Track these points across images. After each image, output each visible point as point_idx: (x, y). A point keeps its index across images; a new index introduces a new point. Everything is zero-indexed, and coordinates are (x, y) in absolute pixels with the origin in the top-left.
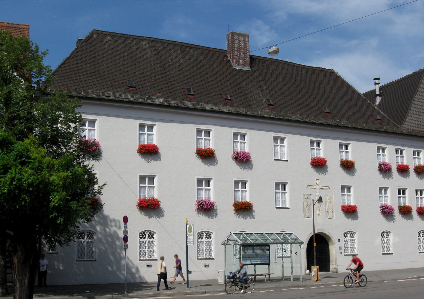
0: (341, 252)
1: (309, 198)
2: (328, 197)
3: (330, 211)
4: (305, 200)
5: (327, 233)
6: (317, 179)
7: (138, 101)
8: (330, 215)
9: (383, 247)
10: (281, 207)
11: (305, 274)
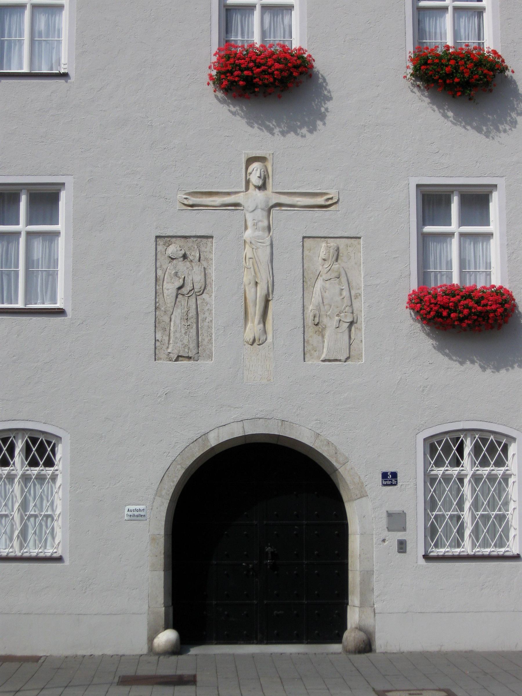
1: (194, 255)
2: (322, 249)
3: (330, 323)
4: (171, 269)
6: (250, 161)
8: (332, 341)
10: (20, 305)
11: (151, 648)
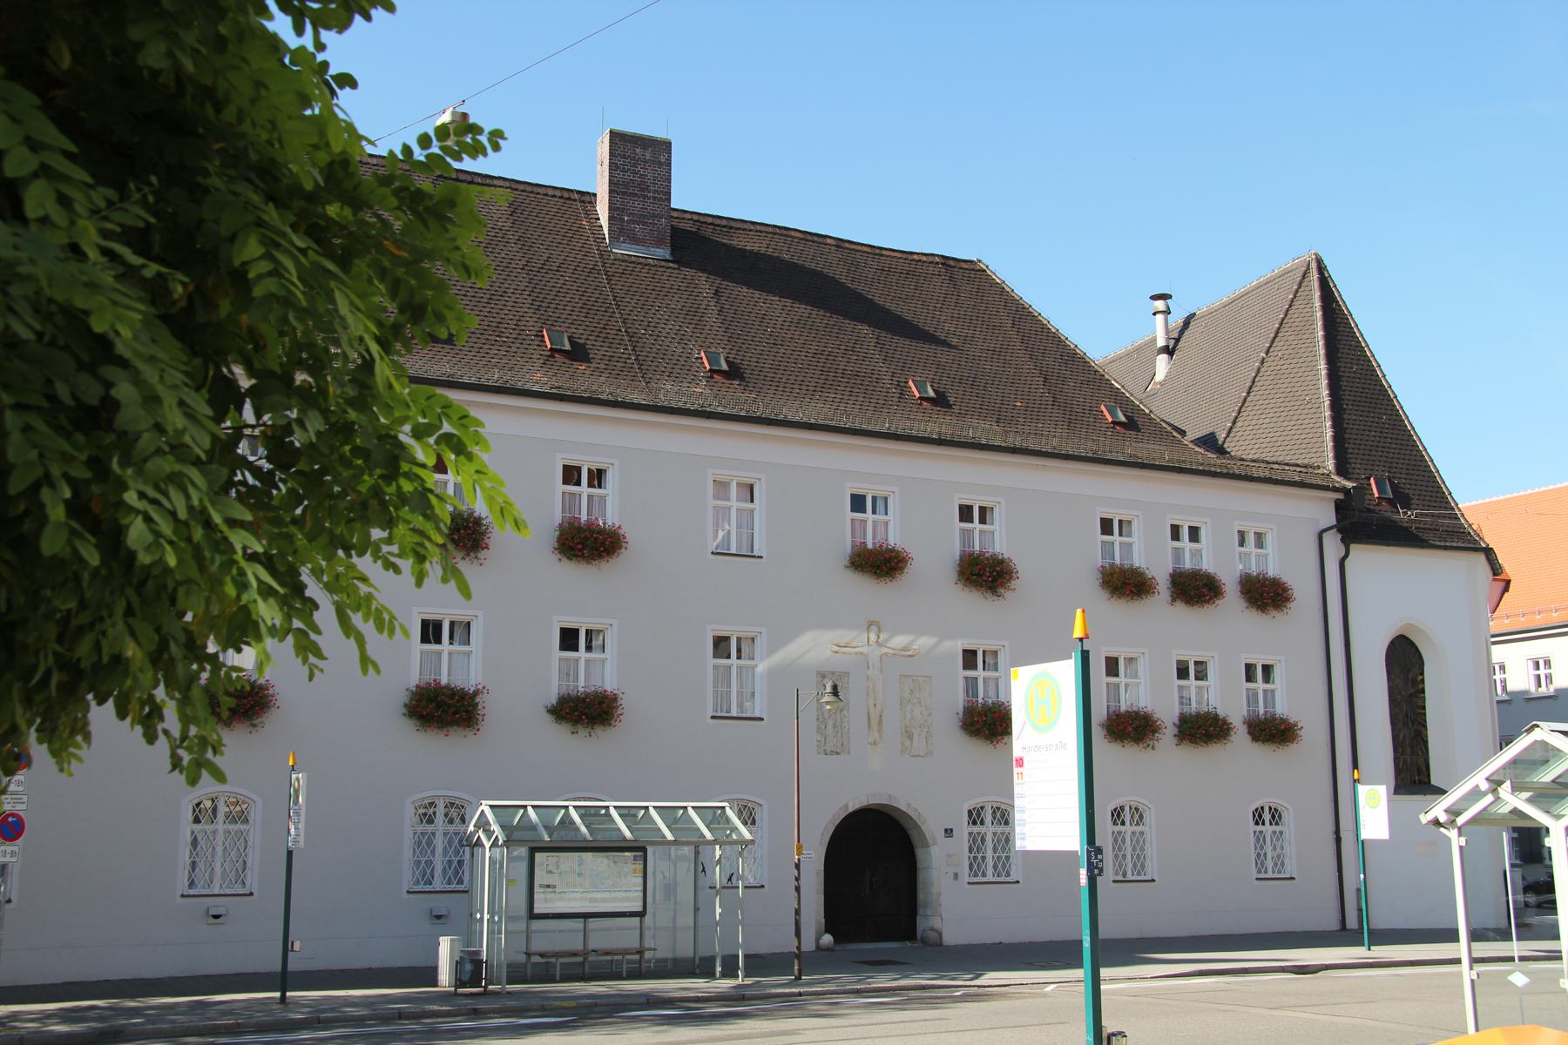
0: (956, 875)
5: (903, 807)
7: (914, 433)
9: (1260, 858)
11: (819, 948)
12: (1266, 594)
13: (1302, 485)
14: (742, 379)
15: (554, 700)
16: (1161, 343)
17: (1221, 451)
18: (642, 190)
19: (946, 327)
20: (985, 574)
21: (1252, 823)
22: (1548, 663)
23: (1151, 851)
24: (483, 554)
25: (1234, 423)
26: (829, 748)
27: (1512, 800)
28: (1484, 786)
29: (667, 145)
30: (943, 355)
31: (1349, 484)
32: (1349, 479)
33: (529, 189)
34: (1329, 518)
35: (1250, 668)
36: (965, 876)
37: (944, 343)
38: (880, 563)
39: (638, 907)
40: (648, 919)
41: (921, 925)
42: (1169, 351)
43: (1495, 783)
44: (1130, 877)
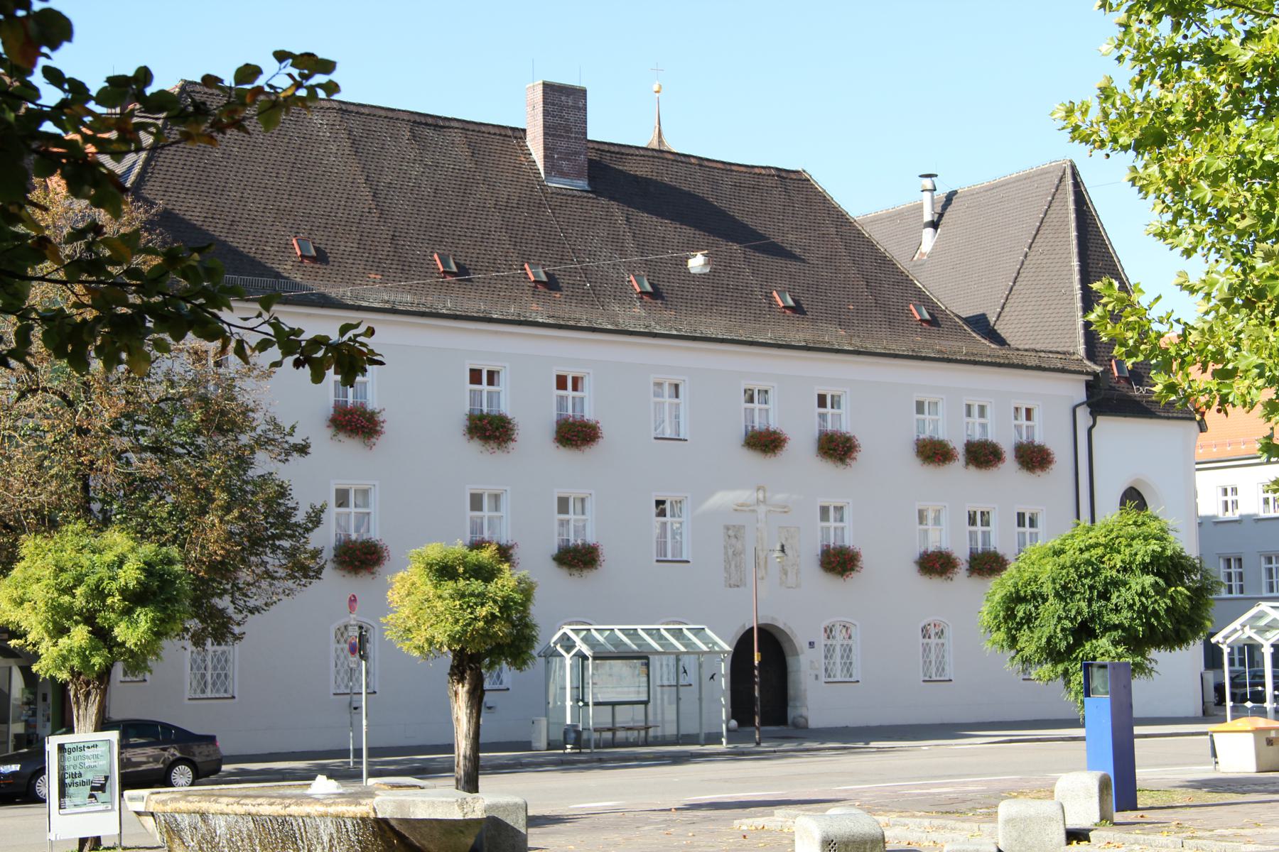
5: (781, 626)
12: (1034, 458)
13: (1063, 371)
14: (662, 298)
15: (556, 551)
16: (928, 217)
17: (993, 336)
18: (567, 132)
19: (790, 239)
20: (837, 448)
21: (921, 636)
22: (1234, 490)
23: (949, 658)
24: (511, 445)
25: (1003, 308)
26: (732, 582)
27: (1249, 632)
28: (1239, 627)
29: (582, 93)
30: (793, 266)
31: (1099, 369)
32: (1095, 363)
33: (476, 128)
34: (1081, 395)
35: (1021, 516)
36: (823, 678)
37: (790, 256)
38: (766, 442)
39: (644, 698)
40: (650, 706)
41: (791, 714)
42: (935, 225)
43: (1243, 626)
44: (934, 678)
